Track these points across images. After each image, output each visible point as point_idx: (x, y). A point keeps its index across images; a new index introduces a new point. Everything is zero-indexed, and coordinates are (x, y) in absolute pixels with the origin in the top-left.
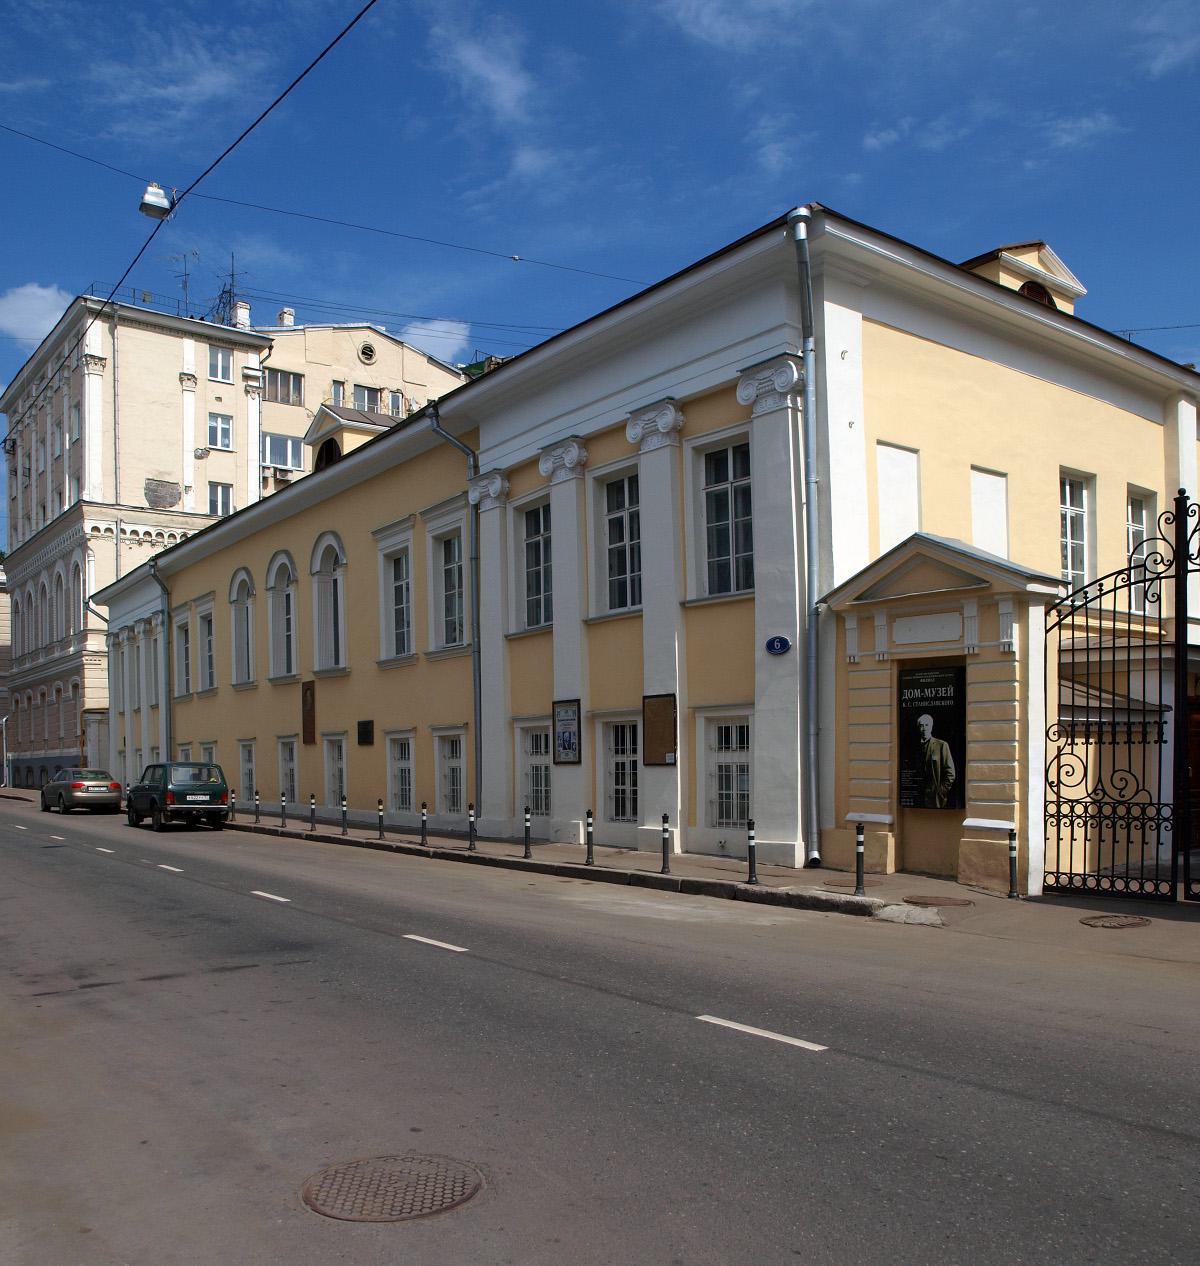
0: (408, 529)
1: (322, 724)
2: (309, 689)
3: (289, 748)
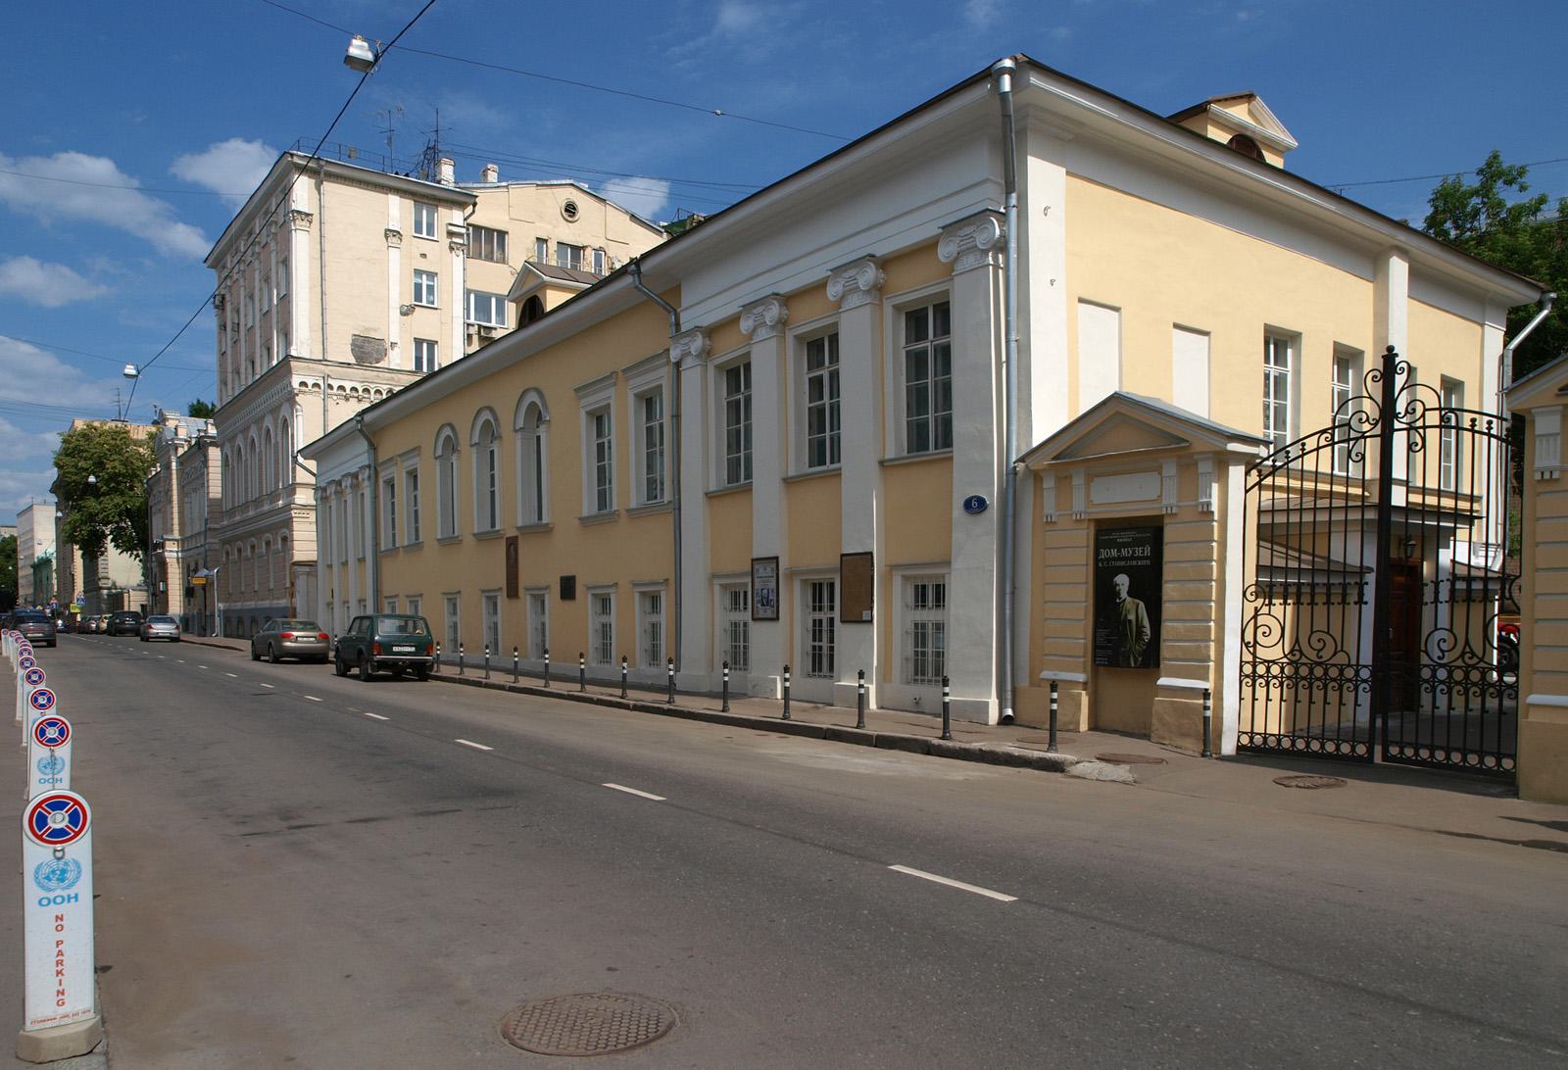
0: (415, 456)
1: (524, 580)
2: (512, 544)
3: (493, 602)
